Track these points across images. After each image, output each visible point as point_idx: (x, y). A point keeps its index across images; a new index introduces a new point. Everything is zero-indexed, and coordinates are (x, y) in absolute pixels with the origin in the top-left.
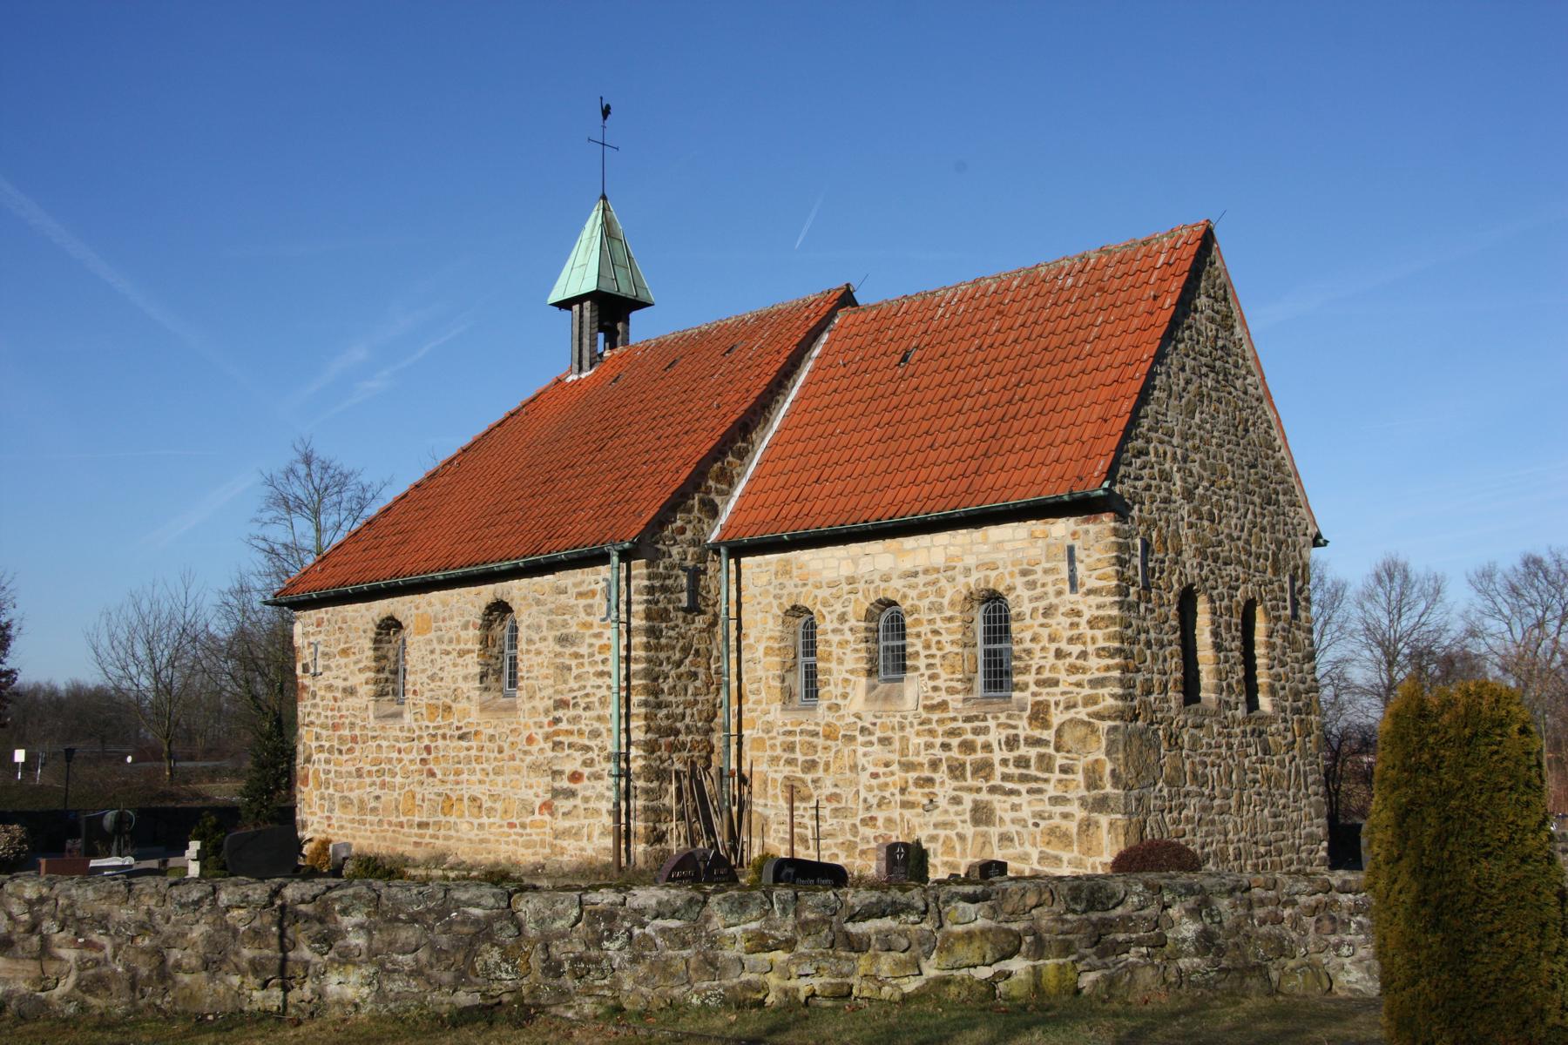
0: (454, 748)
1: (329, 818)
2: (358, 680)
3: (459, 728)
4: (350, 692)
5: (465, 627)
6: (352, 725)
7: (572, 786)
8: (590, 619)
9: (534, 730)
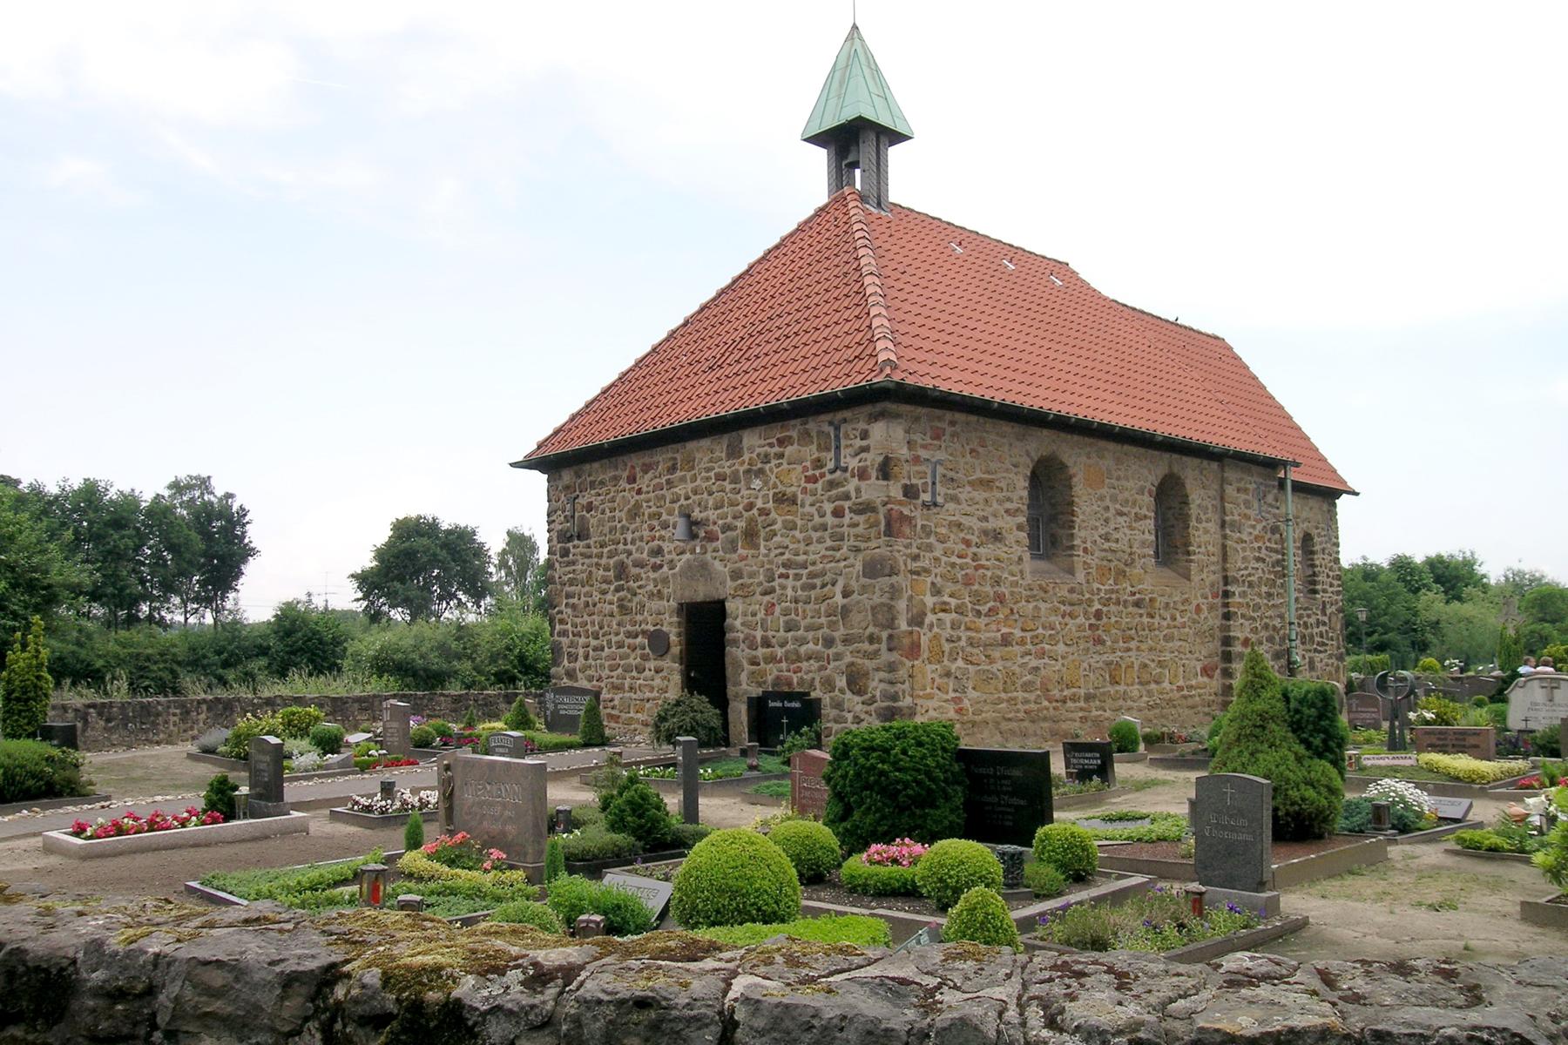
0: (1130, 617)
1: (957, 700)
2: (1007, 523)
3: (1133, 594)
4: (997, 536)
5: (1141, 491)
6: (997, 581)
7: (864, 443)
8: (1248, 512)
9: (1201, 600)
